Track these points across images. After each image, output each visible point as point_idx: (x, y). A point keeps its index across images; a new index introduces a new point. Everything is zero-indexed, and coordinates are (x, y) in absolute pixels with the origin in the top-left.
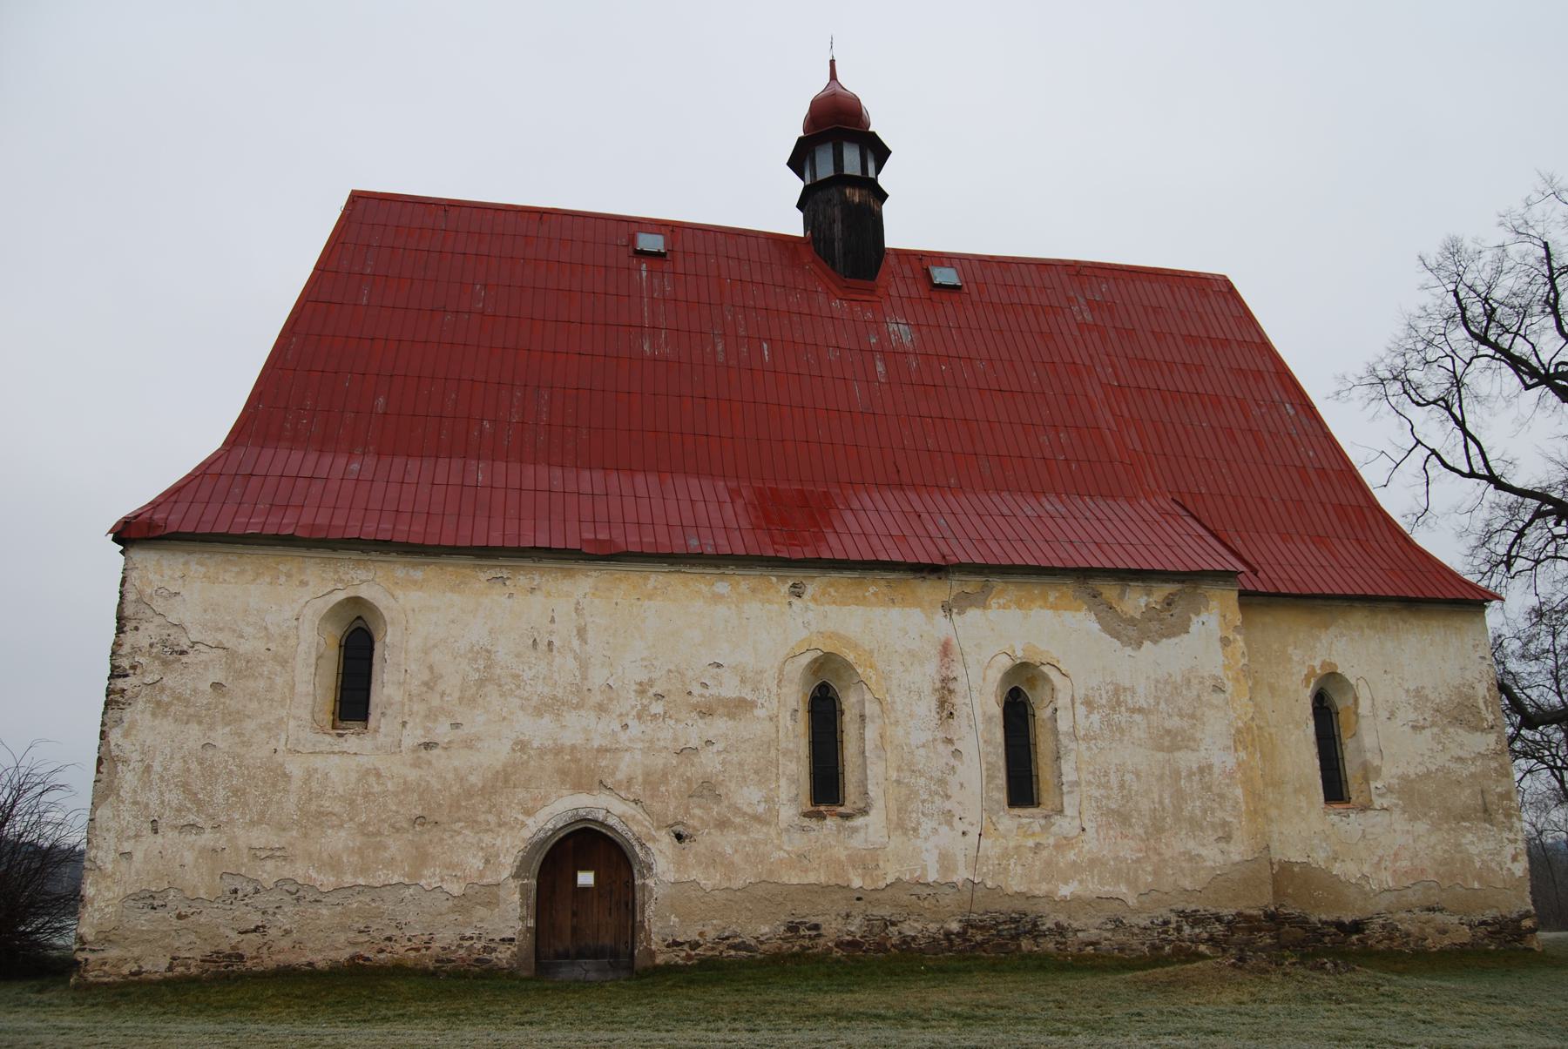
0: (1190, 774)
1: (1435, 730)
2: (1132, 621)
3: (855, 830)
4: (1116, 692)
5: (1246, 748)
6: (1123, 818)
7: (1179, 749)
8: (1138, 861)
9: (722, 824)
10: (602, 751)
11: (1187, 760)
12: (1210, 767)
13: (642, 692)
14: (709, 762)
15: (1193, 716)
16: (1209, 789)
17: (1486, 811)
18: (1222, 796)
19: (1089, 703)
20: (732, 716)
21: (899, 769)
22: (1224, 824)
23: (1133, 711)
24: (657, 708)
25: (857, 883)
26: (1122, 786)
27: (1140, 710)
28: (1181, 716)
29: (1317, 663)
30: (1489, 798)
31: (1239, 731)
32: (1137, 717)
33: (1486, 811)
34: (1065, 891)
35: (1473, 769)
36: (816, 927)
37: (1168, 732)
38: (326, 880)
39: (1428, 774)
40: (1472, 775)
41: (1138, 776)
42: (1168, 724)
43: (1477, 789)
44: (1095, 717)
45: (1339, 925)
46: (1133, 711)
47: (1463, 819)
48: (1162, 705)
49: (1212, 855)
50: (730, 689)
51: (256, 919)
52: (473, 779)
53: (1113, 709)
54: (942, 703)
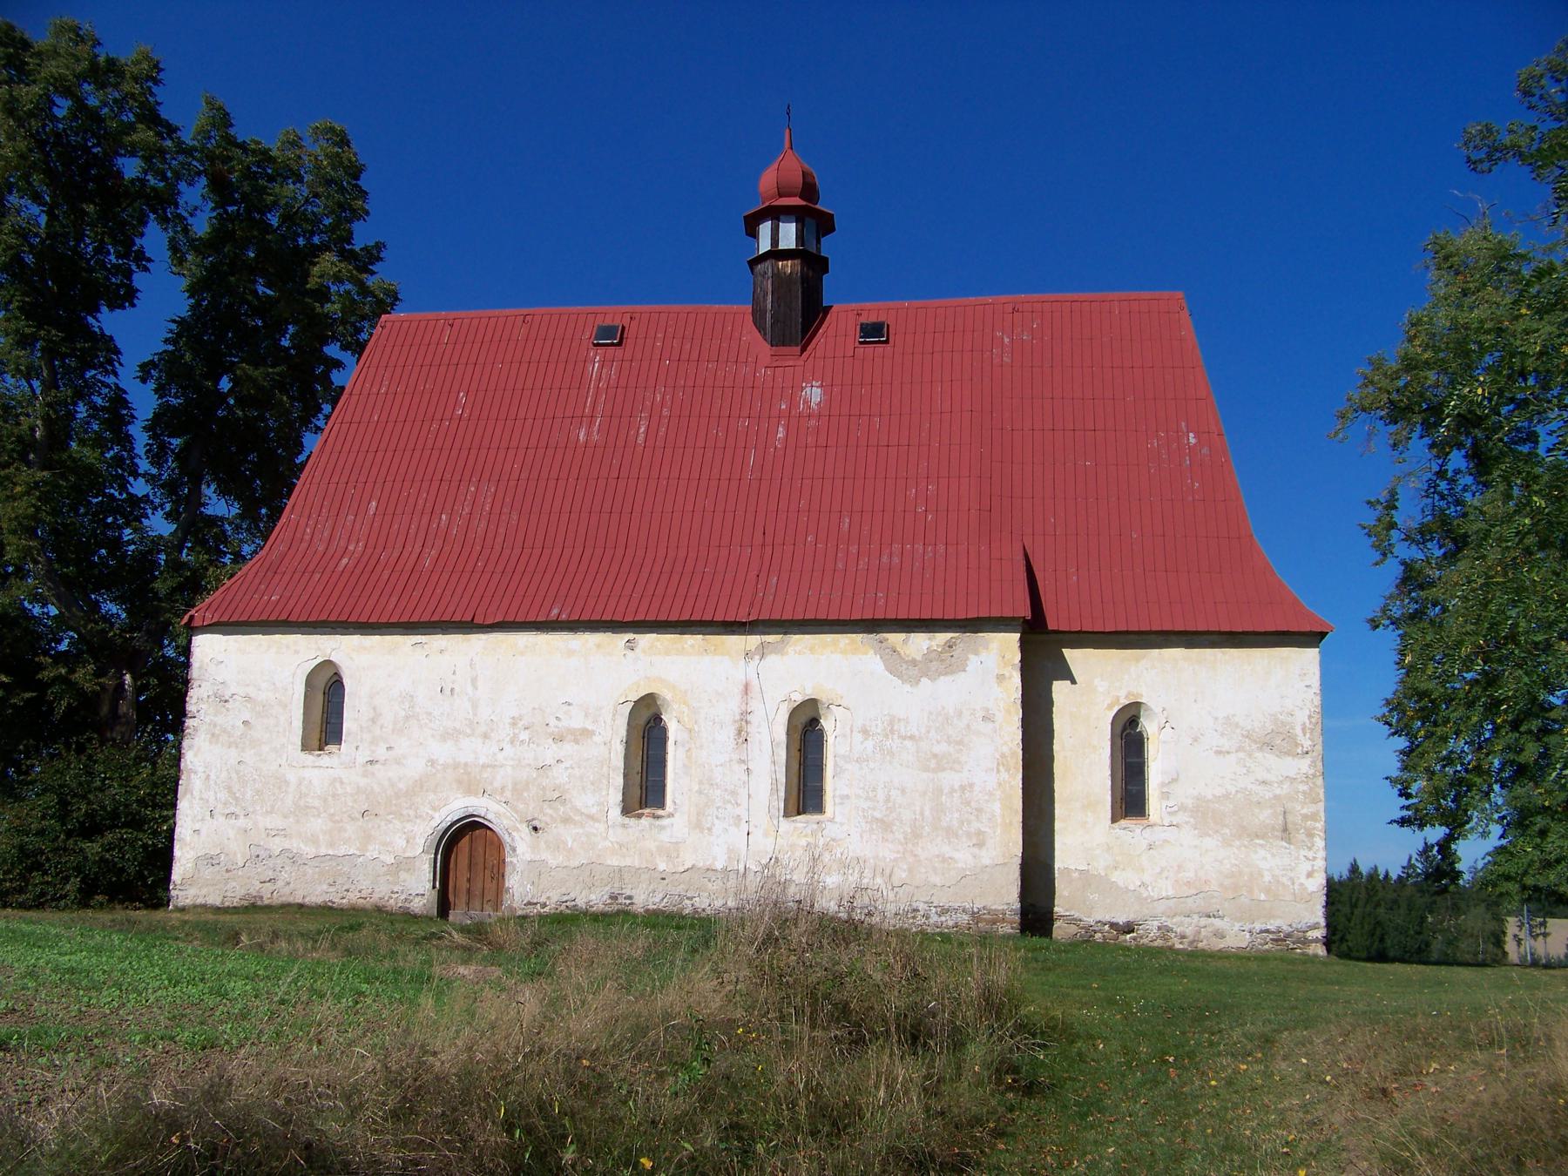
0: (953, 791)
1: (1241, 755)
2: (914, 663)
3: (663, 828)
4: (891, 723)
5: (1008, 770)
6: (885, 826)
7: (944, 770)
8: (895, 860)
9: (566, 820)
10: (484, 766)
11: (950, 779)
12: (971, 785)
13: (514, 724)
14: (560, 775)
15: (960, 743)
16: (968, 803)
17: (1285, 830)
18: (979, 810)
19: (865, 732)
20: (577, 742)
21: (701, 783)
22: (979, 833)
23: (904, 738)
24: (524, 736)
25: (662, 866)
26: (887, 800)
27: (912, 738)
28: (949, 743)
29: (1122, 694)
30: (1290, 818)
31: (1003, 756)
32: (908, 743)
33: (1285, 830)
35: (1278, 791)
36: (630, 898)
37: (935, 756)
38: (309, 850)
39: (1227, 796)
40: (1276, 797)
41: (903, 791)
42: (937, 749)
43: (1280, 810)
44: (870, 744)
45: (1113, 925)
46: (904, 738)
47: (1257, 836)
48: (933, 733)
49: (964, 857)
50: (577, 722)
51: (271, 874)
52: (401, 786)
53: (886, 736)
54: (739, 732)
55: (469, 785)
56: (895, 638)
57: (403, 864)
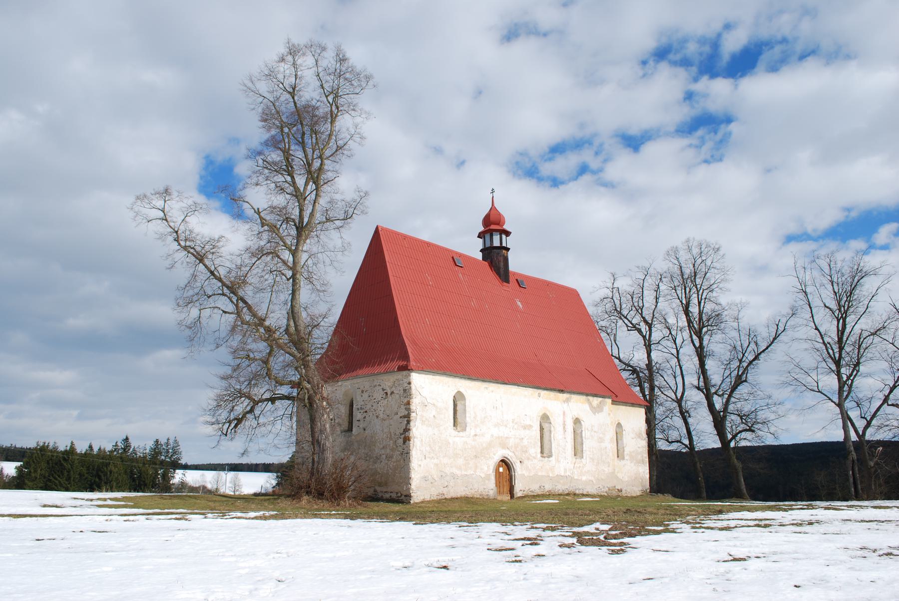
9: (528, 459)
14: (525, 442)
24: (516, 426)
34: (584, 478)
38: (458, 472)
55: (504, 446)
56: (591, 398)
57: (487, 477)
